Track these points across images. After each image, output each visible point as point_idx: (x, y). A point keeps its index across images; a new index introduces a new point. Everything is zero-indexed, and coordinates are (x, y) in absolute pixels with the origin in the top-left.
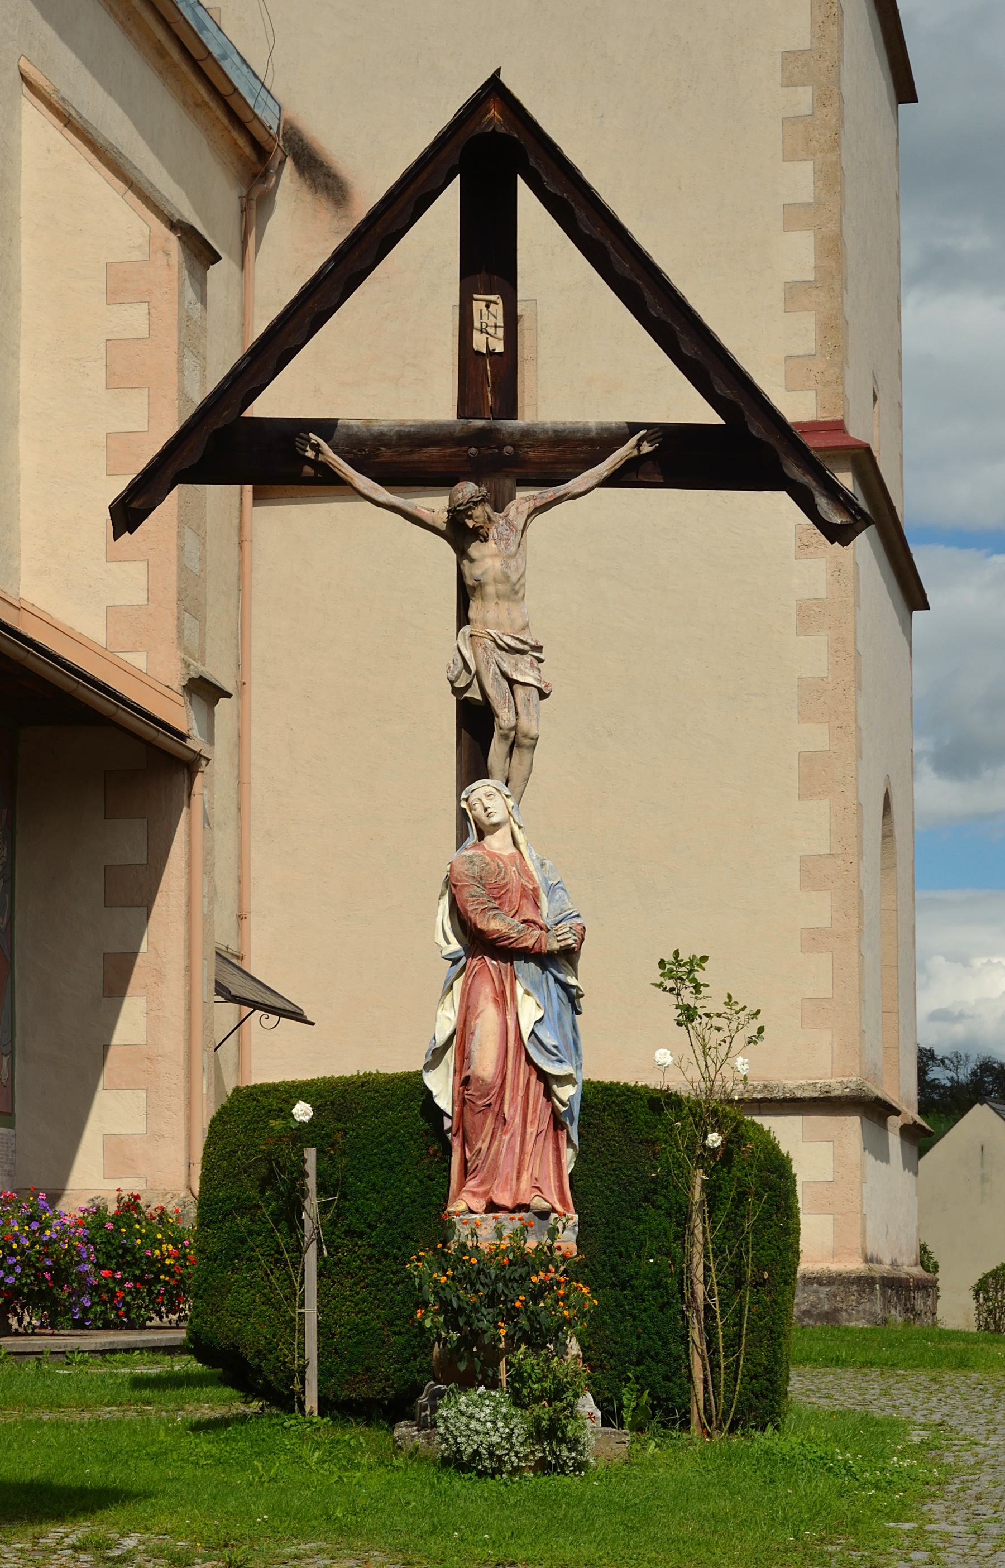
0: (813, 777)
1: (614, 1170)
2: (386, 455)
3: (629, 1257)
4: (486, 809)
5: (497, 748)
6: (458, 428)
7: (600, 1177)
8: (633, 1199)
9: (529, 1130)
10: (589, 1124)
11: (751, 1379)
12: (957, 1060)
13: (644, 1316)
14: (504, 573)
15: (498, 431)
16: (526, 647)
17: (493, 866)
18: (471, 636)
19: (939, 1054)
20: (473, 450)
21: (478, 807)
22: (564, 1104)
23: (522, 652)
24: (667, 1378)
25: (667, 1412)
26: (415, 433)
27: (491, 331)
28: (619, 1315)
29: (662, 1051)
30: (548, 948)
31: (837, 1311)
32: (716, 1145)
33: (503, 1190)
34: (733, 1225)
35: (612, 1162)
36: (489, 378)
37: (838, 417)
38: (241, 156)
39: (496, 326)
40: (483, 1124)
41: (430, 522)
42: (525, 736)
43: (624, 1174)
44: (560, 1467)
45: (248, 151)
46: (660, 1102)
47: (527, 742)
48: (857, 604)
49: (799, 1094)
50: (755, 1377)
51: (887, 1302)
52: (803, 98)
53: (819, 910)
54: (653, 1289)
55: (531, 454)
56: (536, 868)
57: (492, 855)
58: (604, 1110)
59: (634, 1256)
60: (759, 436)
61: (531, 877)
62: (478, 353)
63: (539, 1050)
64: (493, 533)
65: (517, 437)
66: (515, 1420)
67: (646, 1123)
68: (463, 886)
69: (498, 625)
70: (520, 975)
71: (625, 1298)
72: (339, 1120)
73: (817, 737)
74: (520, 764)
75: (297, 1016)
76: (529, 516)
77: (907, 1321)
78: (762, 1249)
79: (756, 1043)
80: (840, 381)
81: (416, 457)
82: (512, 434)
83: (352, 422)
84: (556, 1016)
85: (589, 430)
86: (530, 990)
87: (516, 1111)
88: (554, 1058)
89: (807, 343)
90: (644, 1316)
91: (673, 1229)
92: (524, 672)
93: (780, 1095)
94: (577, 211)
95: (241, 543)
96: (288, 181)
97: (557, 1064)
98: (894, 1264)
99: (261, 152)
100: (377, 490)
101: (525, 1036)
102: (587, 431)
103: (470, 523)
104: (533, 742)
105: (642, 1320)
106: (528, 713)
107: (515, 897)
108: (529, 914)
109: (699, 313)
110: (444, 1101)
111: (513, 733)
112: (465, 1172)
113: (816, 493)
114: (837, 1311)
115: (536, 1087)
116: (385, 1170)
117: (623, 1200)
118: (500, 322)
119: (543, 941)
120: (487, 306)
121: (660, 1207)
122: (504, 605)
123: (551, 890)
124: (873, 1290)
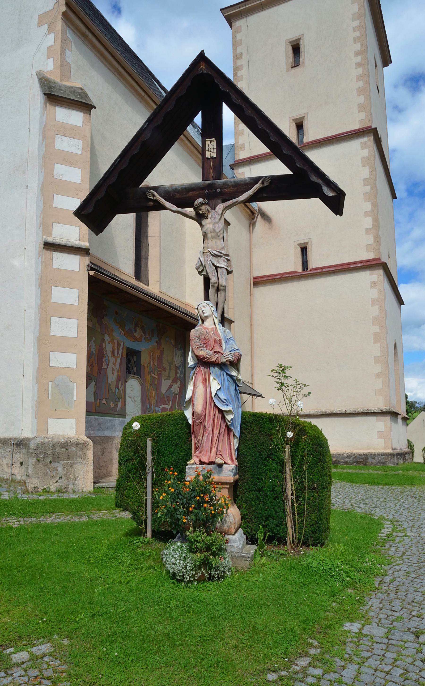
0: (376, 338)
1: (256, 446)
2: (178, 196)
3: (262, 479)
4: (202, 311)
5: (212, 291)
6: (201, 184)
7: (250, 449)
8: (263, 457)
9: (215, 432)
10: (247, 428)
11: (311, 526)
12: (421, 403)
13: (268, 502)
14: (213, 229)
15: (215, 184)
16: (222, 255)
17: (205, 332)
18: (203, 253)
19: (417, 402)
20: (207, 191)
21: (201, 311)
22: (229, 422)
23: (220, 256)
24: (277, 526)
25: (276, 538)
26: (187, 188)
27: (212, 150)
28: (258, 502)
29: (270, 400)
30: (221, 361)
31: (386, 462)
32: (291, 437)
33: (205, 456)
34: (301, 466)
35: (255, 443)
36: (212, 167)
37: (379, 257)
38: (249, 214)
39: (213, 149)
40: (200, 430)
41: (190, 215)
42: (221, 286)
43: (259, 447)
44: (211, 578)
45: (250, 213)
46: (273, 419)
47: (222, 288)
48: (385, 299)
49: (375, 411)
50: (312, 525)
51: (398, 459)
52: (368, 188)
53: (379, 369)
54: (271, 492)
55: (227, 191)
56: (221, 332)
57: (205, 328)
58: (253, 423)
59: (263, 479)
60: (300, 167)
61: (219, 336)
62: (208, 158)
63: (219, 401)
64: (210, 216)
65: (222, 185)
66: (189, 560)
67: (268, 427)
68: (193, 339)
69: (212, 248)
70: (211, 372)
71: (261, 495)
72: (160, 428)
73: (377, 329)
74: (221, 297)
75: (261, 396)
76: (223, 210)
77: (404, 462)
78: (314, 475)
79: (307, 396)
80: (379, 249)
81: (187, 195)
82: (220, 184)
83: (166, 186)
84: (227, 387)
85: (246, 180)
86: (215, 378)
87: (210, 425)
88: (225, 404)
89: (371, 241)
90: (268, 502)
91: (278, 468)
92: (222, 263)
93: (371, 412)
94: (232, 95)
95: (251, 295)
96: (259, 220)
97: (226, 406)
98: (401, 449)
99: (253, 213)
100: (173, 207)
101: (213, 396)
102: (245, 180)
103: (201, 212)
104: (224, 288)
105: (267, 503)
106: (222, 277)
107: (212, 343)
108: (217, 349)
109: (276, 124)
110: (190, 422)
111: (216, 285)
112: (196, 448)
113: (323, 186)
114: (386, 462)
115: (218, 416)
116: (174, 446)
117: (259, 457)
118: (215, 147)
119: (219, 358)
120: (211, 143)
121: (274, 460)
122: (214, 240)
123: (227, 341)
124: (394, 457)
